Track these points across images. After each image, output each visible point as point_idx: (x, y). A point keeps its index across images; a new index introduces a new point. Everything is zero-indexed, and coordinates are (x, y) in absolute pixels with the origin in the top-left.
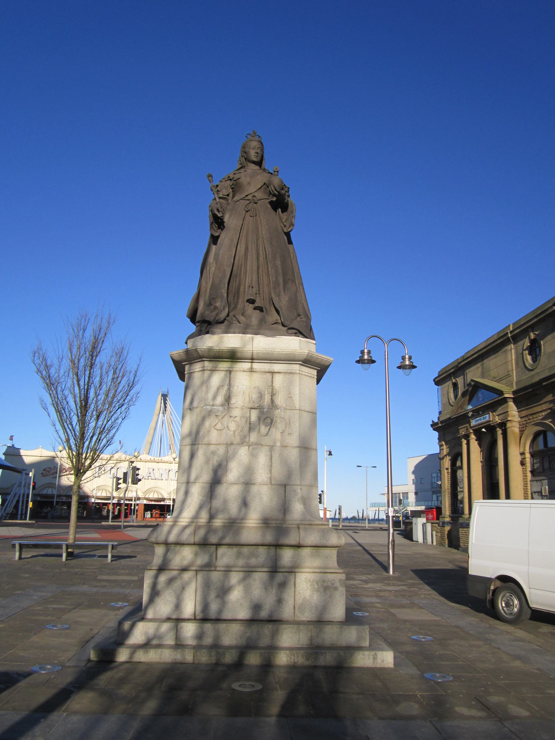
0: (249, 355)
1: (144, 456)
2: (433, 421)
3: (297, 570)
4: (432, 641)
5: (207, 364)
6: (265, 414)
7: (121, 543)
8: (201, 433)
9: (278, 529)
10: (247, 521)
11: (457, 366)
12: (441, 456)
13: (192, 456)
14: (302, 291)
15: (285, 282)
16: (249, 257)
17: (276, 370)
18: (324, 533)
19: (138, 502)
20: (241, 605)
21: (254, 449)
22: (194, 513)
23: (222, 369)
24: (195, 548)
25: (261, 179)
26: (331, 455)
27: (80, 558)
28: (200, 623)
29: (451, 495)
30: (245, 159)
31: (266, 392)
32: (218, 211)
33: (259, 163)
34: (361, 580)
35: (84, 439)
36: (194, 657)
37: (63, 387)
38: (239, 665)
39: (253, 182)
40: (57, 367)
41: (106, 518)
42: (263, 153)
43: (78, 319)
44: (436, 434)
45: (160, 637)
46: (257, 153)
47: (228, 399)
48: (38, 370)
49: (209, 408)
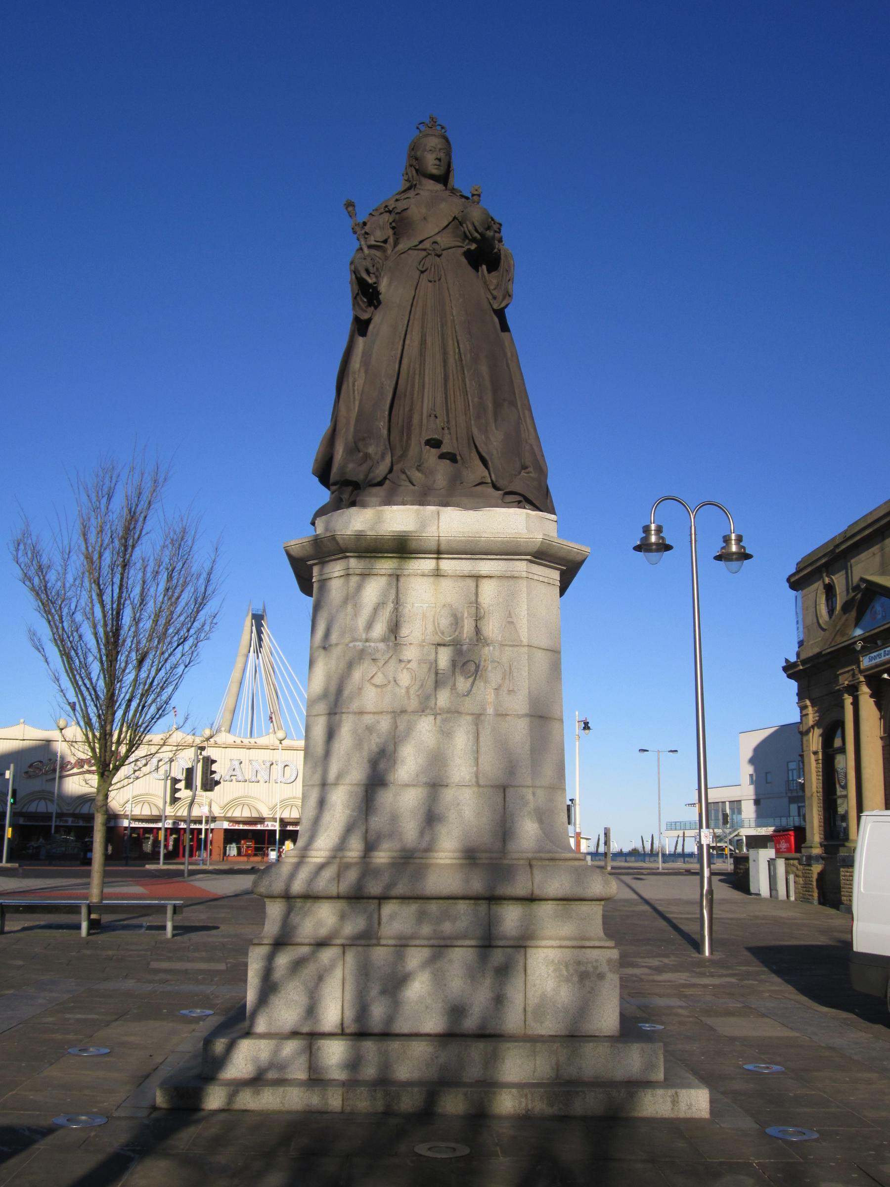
0: (433, 545)
1: (223, 737)
2: (787, 661)
3: (529, 943)
4: (782, 1073)
5: (353, 562)
6: (465, 655)
7: (190, 902)
8: (346, 693)
9: (493, 866)
10: (436, 855)
11: (832, 551)
12: (804, 728)
13: (331, 734)
14: (528, 420)
15: (497, 406)
16: (428, 359)
17: (483, 573)
18: (580, 874)
19: (212, 826)
20: (427, 1007)
21: (445, 721)
22: (337, 840)
23: (383, 572)
24: (341, 905)
25: (448, 208)
26: (589, 728)
27: (114, 930)
28: (352, 1040)
29: (824, 803)
30: (417, 170)
31: (466, 615)
32: (368, 272)
33: (443, 179)
34: (649, 967)
35: (113, 706)
36: (343, 1101)
37: (73, 607)
38: (427, 1114)
39: (432, 215)
40: (59, 568)
41: (154, 857)
42: (450, 157)
43: (97, 476)
44: (793, 685)
45: (282, 1067)
46: (440, 160)
47: (394, 628)
48: (26, 575)
49: (360, 645)
